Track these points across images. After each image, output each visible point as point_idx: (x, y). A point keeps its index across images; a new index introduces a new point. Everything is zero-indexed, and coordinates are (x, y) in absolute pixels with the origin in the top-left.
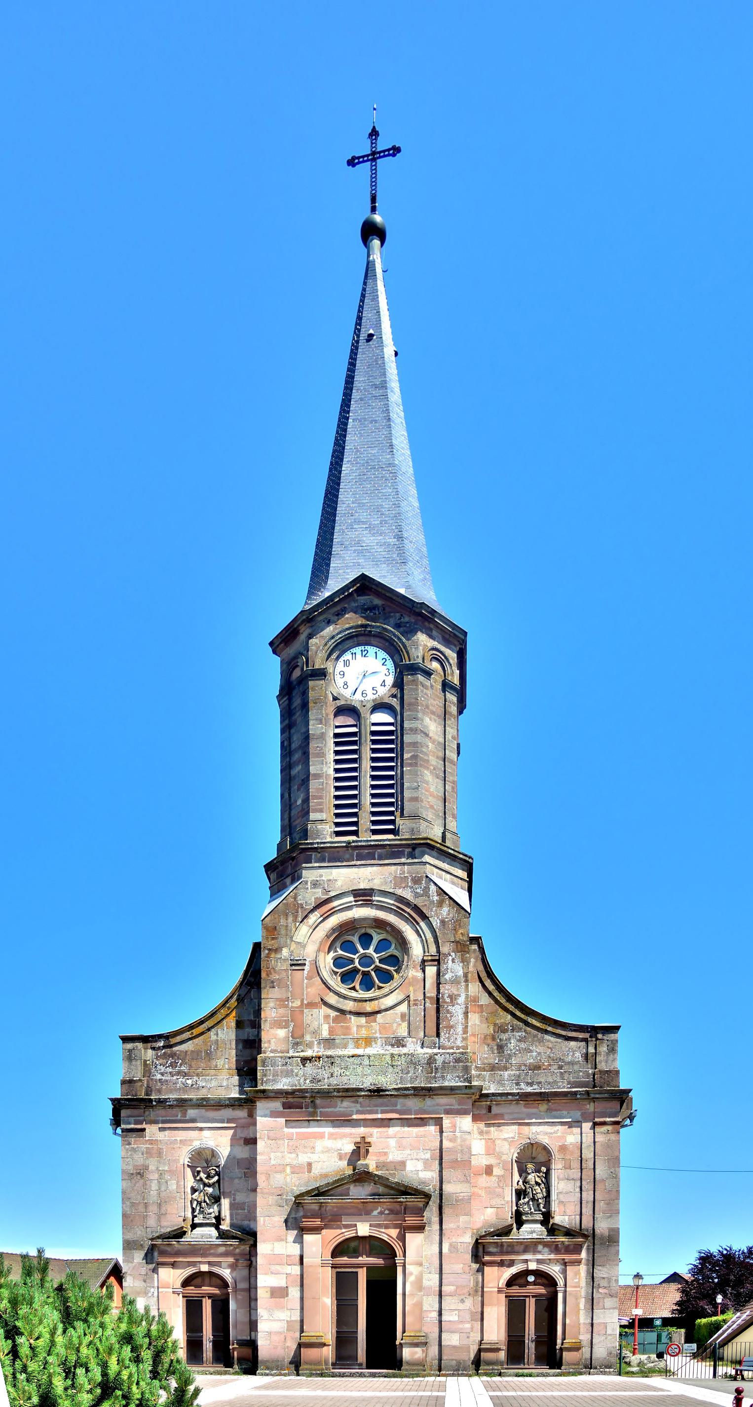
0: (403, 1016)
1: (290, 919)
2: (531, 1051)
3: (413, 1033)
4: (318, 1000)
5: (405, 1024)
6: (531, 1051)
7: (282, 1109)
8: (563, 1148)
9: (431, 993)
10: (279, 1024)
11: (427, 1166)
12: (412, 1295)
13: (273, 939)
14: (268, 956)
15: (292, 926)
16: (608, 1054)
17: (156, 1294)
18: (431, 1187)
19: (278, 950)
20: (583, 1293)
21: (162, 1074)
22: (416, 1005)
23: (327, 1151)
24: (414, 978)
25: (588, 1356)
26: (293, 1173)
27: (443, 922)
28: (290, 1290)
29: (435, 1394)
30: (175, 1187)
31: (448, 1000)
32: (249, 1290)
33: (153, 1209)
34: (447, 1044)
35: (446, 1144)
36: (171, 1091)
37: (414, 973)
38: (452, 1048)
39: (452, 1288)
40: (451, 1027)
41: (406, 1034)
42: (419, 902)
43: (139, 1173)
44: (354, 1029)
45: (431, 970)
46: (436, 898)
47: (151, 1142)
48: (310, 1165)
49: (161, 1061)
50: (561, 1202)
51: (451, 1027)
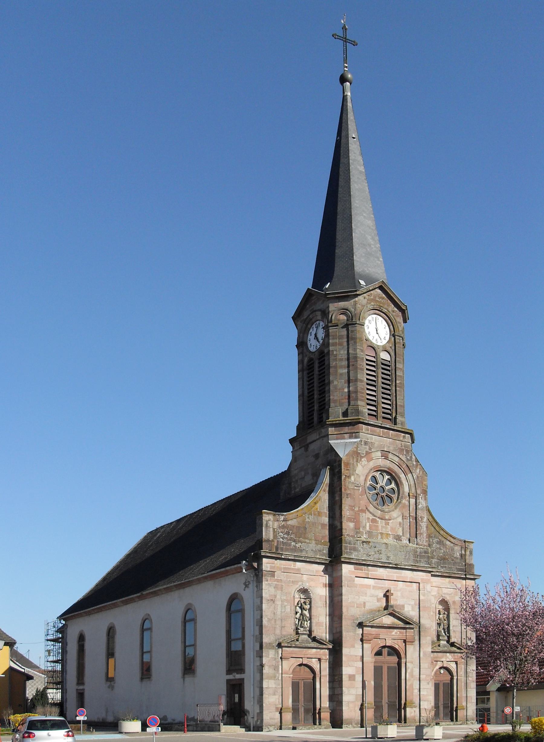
0: (400, 524)
1: (355, 460)
2: (441, 549)
3: (405, 534)
4: (365, 508)
5: (401, 529)
6: (441, 549)
7: (353, 570)
8: (454, 602)
9: (413, 514)
10: (350, 520)
11: (413, 610)
12: (409, 680)
13: (347, 470)
14: (345, 479)
15: (355, 463)
16: (469, 556)
17: (280, 678)
18: (416, 619)
19: (349, 477)
20: (463, 680)
21: (283, 538)
22: (406, 519)
23: (372, 596)
24: (405, 504)
25: (465, 714)
26: (357, 607)
27: (418, 477)
28: (356, 676)
29: (186, 726)
30: (289, 610)
31: (420, 519)
32: (334, 675)
33: (278, 622)
34: (421, 543)
35: (421, 598)
36: (287, 550)
37: (405, 501)
38: (422, 545)
39: (424, 676)
40: (421, 534)
41: (401, 534)
42: (409, 464)
43: (272, 600)
44: (380, 527)
45: (413, 501)
46: (415, 463)
47: (278, 581)
48: (364, 603)
49: (281, 530)
50: (454, 631)
51: (421, 534)
